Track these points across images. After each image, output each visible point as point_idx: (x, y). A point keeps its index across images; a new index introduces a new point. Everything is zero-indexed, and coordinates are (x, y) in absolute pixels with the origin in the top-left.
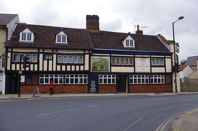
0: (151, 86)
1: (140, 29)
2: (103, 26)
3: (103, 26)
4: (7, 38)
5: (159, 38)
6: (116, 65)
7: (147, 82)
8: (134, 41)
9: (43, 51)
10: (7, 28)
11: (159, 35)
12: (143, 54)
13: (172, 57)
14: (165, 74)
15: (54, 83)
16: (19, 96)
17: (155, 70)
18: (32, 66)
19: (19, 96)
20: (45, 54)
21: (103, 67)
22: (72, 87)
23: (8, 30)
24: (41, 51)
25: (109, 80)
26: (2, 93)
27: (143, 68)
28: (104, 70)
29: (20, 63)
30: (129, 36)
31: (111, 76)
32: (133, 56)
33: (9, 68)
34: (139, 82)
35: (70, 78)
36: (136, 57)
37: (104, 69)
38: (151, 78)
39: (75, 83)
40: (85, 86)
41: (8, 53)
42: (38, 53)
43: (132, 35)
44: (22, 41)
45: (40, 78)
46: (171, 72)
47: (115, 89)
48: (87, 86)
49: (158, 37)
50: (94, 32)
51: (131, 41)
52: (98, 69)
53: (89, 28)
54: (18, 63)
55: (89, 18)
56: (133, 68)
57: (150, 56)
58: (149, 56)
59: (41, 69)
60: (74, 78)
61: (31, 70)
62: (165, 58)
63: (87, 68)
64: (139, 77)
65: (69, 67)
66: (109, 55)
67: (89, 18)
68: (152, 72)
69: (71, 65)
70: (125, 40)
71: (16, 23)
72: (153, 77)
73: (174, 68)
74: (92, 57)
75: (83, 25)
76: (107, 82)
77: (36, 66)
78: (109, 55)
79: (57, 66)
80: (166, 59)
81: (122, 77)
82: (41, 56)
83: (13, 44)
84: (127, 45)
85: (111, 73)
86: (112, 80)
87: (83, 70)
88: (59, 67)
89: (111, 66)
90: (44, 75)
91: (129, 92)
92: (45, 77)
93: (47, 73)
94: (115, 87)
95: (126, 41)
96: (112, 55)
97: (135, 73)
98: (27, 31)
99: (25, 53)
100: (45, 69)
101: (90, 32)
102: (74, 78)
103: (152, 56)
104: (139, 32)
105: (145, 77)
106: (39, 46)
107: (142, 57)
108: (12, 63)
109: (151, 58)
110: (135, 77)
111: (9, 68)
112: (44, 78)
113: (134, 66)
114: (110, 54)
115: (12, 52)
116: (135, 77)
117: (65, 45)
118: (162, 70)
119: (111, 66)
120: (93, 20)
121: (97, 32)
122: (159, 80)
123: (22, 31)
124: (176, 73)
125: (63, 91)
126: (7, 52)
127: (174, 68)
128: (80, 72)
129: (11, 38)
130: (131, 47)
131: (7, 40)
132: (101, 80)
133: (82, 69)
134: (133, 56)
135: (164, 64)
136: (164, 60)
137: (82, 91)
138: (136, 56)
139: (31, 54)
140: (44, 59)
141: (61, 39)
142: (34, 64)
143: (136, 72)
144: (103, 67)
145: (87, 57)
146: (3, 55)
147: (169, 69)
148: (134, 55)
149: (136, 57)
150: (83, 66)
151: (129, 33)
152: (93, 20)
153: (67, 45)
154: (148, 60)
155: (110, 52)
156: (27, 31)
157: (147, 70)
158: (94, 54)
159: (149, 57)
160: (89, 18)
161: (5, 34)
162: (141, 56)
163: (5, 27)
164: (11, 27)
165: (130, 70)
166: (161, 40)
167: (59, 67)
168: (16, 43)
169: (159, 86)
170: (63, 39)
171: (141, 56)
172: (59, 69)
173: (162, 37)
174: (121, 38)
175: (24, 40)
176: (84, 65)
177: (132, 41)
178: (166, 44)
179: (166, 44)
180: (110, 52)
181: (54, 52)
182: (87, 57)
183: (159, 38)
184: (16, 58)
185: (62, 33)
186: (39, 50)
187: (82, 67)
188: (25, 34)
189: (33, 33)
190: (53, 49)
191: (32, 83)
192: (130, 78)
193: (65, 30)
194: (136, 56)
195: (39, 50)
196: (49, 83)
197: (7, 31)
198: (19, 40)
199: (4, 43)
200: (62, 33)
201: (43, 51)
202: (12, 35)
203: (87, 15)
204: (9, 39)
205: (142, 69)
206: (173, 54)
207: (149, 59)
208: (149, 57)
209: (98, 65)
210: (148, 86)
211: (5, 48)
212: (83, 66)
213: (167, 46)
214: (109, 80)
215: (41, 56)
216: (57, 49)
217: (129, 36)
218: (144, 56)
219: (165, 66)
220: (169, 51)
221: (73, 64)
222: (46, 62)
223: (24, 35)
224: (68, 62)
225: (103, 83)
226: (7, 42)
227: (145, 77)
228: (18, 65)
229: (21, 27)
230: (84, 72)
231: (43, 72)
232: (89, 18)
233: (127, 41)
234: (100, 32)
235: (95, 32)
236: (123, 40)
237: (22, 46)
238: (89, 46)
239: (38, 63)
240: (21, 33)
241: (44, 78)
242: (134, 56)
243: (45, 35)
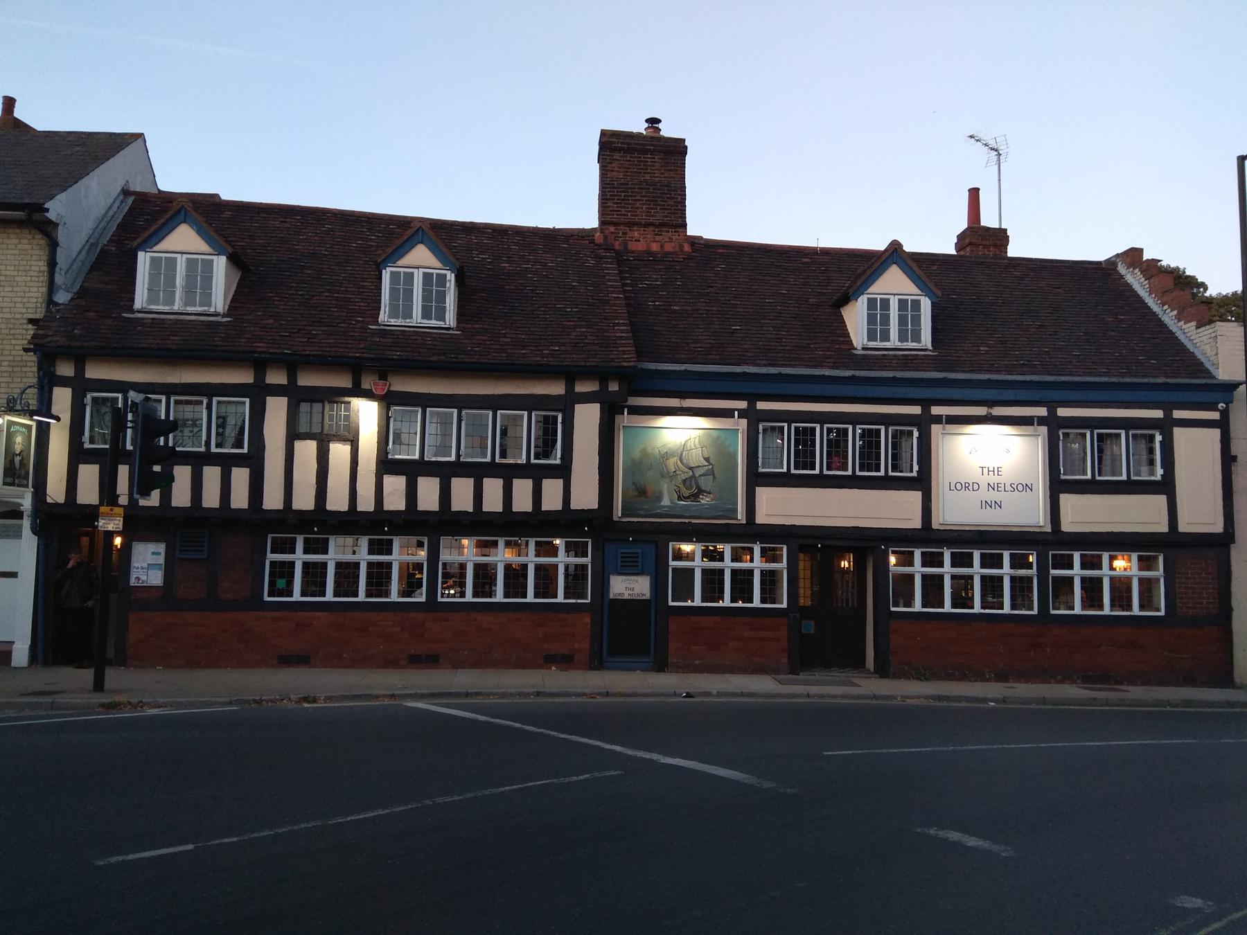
1: (988, 219)
2: (720, 208)
3: (720, 208)
4: (52, 287)
5: (1135, 280)
9: (292, 378)
10: (56, 225)
11: (1133, 256)
12: (991, 400)
13: (1225, 414)
14: (1168, 545)
15: (721, 604)
16: (99, 685)
17: (1082, 513)
18: (182, 474)
19: (99, 685)
20: (297, 397)
21: (700, 491)
23: (61, 235)
25: (992, 586)
26: (10, 653)
31: (1077, 557)
32: (916, 410)
33: (56, 490)
35: (728, 564)
36: (938, 420)
37: (705, 500)
38: (1054, 572)
39: (336, 594)
41: (579, 408)
42: (258, 394)
43: (923, 267)
45: (272, 557)
48: (588, 620)
49: (1122, 269)
50: (649, 253)
52: (666, 502)
53: (616, 224)
55: (617, 150)
57: (1052, 411)
59: (273, 499)
61: (233, 506)
62: (1166, 426)
63: (586, 496)
64: (962, 560)
65: (462, 491)
66: (743, 405)
67: (619, 150)
68: (1183, 528)
69: (445, 473)
70: (862, 301)
71: (126, 192)
72: (1071, 567)
74: (625, 419)
75: (567, 199)
77: (240, 477)
78: (1042, 411)
80: (1177, 431)
82: (276, 409)
83: (89, 325)
84: (871, 335)
85: (752, 533)
86: (762, 582)
88: (395, 486)
89: (756, 479)
90: (294, 541)
91: (882, 670)
92: (306, 551)
93: (321, 524)
95: (872, 303)
97: (928, 537)
98: (184, 240)
99: (169, 390)
100: (304, 500)
101: (618, 253)
103: (1062, 412)
104: (983, 241)
106: (261, 346)
111: (56, 490)
112: (299, 557)
114: (752, 398)
115: (80, 386)
116: (932, 560)
118: (1144, 513)
119: (756, 479)
120: (643, 168)
121: (669, 248)
122: (515, 576)
123: (147, 244)
126: (48, 381)
128: (538, 525)
129: (82, 293)
130: (427, 323)
131: (50, 302)
133: (552, 497)
134: (916, 410)
136: (916, 434)
138: (1177, 414)
139: (205, 401)
140: (293, 435)
141: (416, 296)
142: (227, 463)
143: (935, 526)
144: (700, 491)
145: (587, 417)
146: (9, 401)
149: (938, 420)
150: (561, 481)
151: (895, 247)
152: (643, 168)
156: (184, 240)
159: (1042, 421)
160: (619, 150)
161: (39, 265)
163: (37, 216)
164: (82, 209)
165: (896, 509)
166: (1143, 293)
167: (395, 486)
168: (109, 322)
172: (395, 500)
173: (1153, 269)
175: (404, 317)
176: (564, 471)
178: (1179, 318)
179: (1179, 318)
182: (587, 417)
183: (1130, 279)
184: (905, 455)
185: (421, 257)
188: (885, 304)
189: (223, 259)
193: (443, 234)
194: (1177, 414)
195: (260, 376)
197: (53, 245)
198: (133, 300)
200: (421, 257)
201: (292, 378)
202: (93, 268)
203: (604, 133)
204: (62, 297)
208: (1042, 421)
209: (663, 476)
210: (420, 616)
211: (32, 358)
212: (561, 481)
213: (1189, 333)
214: (742, 581)
215: (276, 409)
219: (1166, 487)
220: (1207, 373)
221: (491, 470)
222: (306, 450)
223: (163, 269)
224: (458, 455)
225: (697, 601)
226: (49, 316)
228: (212, 475)
229: (151, 213)
230: (568, 522)
231: (290, 523)
232: (617, 150)
233: (878, 309)
234: (687, 248)
235: (655, 247)
236: (846, 299)
239: (255, 461)
240: (141, 255)
241: (299, 557)
242: (1168, 414)
243: (307, 281)
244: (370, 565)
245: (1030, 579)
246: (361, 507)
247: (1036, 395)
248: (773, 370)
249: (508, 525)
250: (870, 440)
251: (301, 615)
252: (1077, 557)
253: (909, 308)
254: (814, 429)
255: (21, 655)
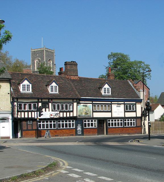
0: (125, 129)
6: (97, 111)
7: (54, 127)
8: (110, 89)
9: (42, 100)
12: (118, 101)
14: (136, 118)
17: (128, 115)
22: (63, 130)
24: (40, 100)
27: (119, 113)
28: (87, 116)
29: (28, 111)
30: (106, 84)
31: (87, 120)
34: (66, 126)
35: (87, 122)
38: (125, 122)
40: (73, 130)
44: (27, 91)
46: (140, 116)
47: (97, 132)
51: (27, 85)
54: (26, 111)
56: (111, 113)
57: (124, 103)
58: (123, 103)
60: (64, 123)
62: (111, 104)
63: (75, 115)
64: (115, 121)
67: (69, 64)
68: (137, 116)
72: (89, 122)
73: (143, 113)
76: (62, 125)
79: (94, 113)
81: (101, 121)
85: (93, 118)
87: (124, 117)
89: (93, 112)
94: (97, 130)
96: (93, 102)
97: (112, 118)
102: (64, 123)
103: (125, 103)
105: (120, 121)
106: (39, 97)
107: (118, 104)
108: (18, 111)
109: (124, 104)
110: (112, 121)
113: (111, 111)
114: (92, 101)
117: (28, 94)
118: (133, 115)
119: (93, 112)
124: (144, 117)
125: (56, 134)
127: (143, 113)
130: (27, 91)
132: (85, 124)
133: (71, 115)
134: (110, 103)
135: (110, 110)
136: (110, 106)
137: (71, 134)
138: (112, 103)
147: (139, 114)
148: (111, 102)
153: (58, 95)
154: (122, 106)
155: (92, 100)
157: (122, 115)
158: (81, 102)
162: (117, 103)
169: (131, 128)
170: (25, 88)
171: (117, 103)
174: (98, 85)
176: (73, 111)
177: (109, 89)
180: (92, 100)
181: (50, 101)
182: (75, 104)
183: (130, 83)
186: (38, 100)
187: (71, 113)
190: (73, 99)
191: (32, 128)
192: (108, 122)
194: (112, 103)
195: (38, 100)
196: (53, 128)
199: (8, 93)
201: (42, 100)
205: (118, 114)
206: (143, 100)
207: (123, 105)
216: (52, 99)
217: (106, 84)
218: (119, 103)
227: (120, 121)
228: (26, 113)
235: (74, 79)
236: (19, 84)
237: (26, 97)
238: (76, 95)
242: (111, 103)
244: (130, 122)
245: (55, 124)
246: (64, 116)
247: (91, 100)
248: (103, 98)
249: (67, 119)
250: (130, 106)
251: (128, 128)
252: (90, 120)
253: (28, 86)
254: (22, 104)
255: (11, 137)
